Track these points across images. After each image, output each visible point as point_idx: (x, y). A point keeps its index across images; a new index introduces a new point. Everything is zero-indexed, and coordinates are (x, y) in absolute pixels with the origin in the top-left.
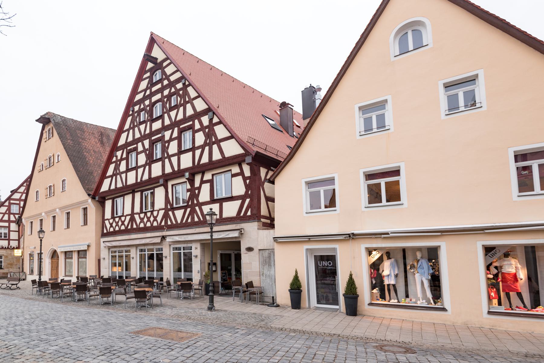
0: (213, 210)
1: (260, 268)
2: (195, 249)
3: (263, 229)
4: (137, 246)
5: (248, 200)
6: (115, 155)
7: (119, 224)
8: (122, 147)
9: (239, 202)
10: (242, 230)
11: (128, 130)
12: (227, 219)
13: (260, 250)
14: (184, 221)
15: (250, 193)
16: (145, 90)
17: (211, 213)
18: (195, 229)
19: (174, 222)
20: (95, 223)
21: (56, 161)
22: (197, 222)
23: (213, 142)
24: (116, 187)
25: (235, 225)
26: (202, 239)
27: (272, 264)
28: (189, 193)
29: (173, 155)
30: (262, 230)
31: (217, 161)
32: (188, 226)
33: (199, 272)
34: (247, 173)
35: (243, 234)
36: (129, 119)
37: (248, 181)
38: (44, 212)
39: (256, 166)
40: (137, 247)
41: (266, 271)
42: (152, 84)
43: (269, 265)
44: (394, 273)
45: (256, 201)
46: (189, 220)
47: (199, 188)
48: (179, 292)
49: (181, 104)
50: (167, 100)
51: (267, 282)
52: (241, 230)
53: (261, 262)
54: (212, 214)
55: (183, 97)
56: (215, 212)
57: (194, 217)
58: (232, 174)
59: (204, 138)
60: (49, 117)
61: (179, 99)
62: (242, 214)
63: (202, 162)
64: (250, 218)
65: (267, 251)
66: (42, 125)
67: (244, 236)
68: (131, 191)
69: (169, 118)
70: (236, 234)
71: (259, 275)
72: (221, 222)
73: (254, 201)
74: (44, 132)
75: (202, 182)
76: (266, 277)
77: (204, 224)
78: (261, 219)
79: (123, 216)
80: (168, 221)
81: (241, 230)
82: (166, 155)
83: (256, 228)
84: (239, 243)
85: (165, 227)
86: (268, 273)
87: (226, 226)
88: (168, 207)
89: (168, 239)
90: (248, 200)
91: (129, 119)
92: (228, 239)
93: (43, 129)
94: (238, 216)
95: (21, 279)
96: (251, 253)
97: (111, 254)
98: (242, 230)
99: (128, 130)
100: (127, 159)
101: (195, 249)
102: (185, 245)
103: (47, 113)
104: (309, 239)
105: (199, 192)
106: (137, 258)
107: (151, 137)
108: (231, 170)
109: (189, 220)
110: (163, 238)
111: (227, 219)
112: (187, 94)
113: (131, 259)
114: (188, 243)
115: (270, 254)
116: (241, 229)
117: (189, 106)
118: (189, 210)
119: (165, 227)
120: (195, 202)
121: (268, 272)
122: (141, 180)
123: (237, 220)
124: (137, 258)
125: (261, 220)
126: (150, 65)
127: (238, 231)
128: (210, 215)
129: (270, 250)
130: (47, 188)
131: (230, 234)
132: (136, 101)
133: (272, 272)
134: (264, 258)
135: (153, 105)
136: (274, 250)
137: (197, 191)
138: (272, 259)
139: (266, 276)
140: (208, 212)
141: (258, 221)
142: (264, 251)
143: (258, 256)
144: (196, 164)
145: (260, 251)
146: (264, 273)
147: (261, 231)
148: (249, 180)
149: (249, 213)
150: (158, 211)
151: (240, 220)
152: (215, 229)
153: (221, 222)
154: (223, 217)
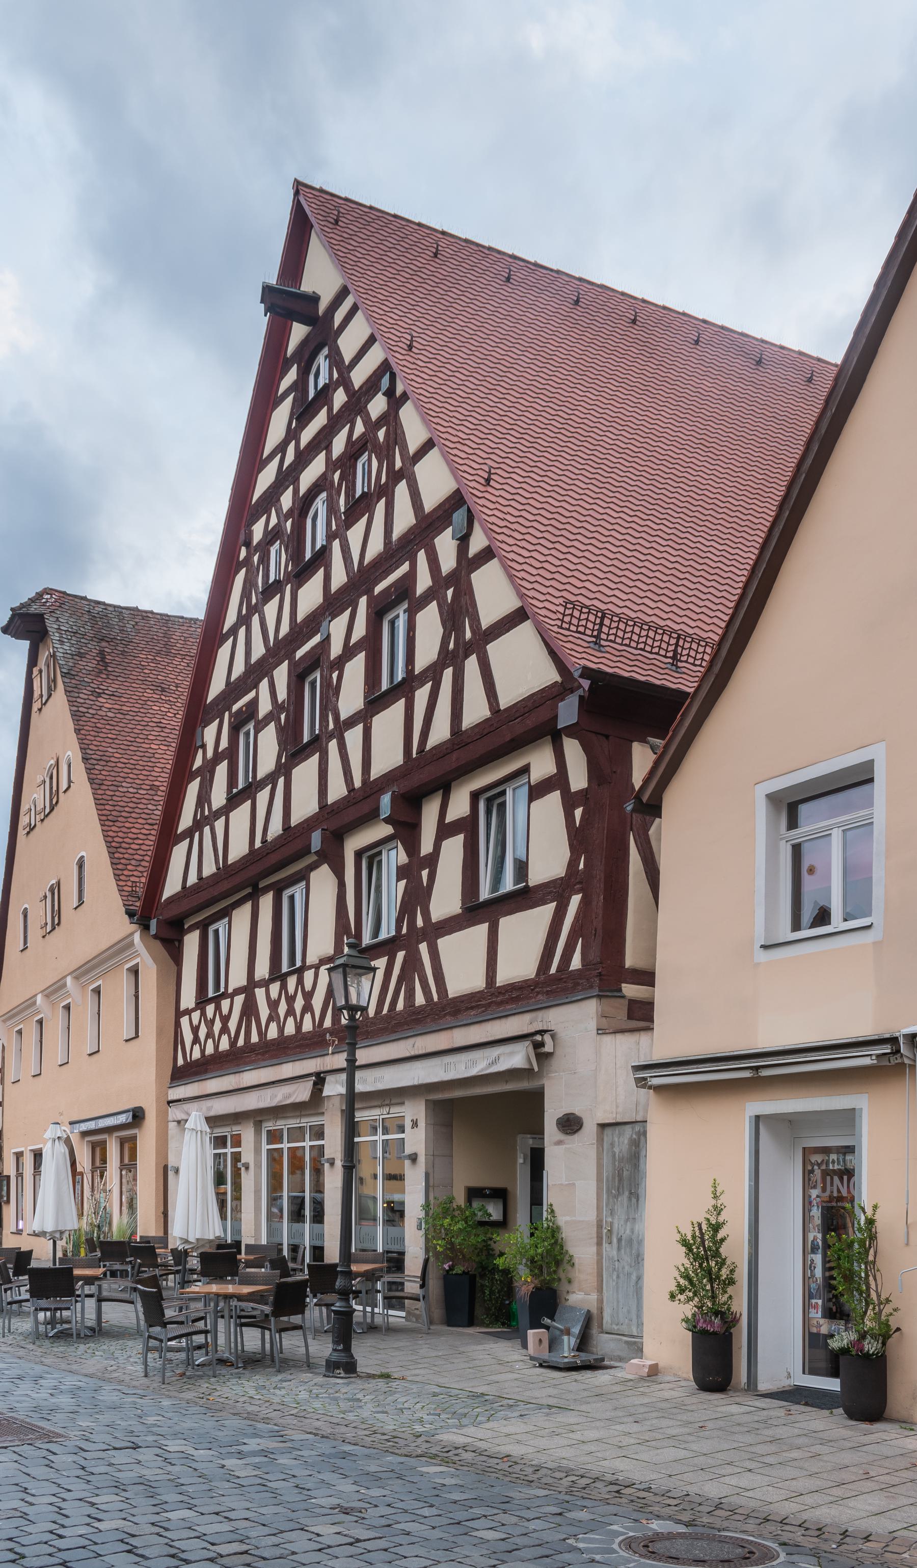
1: (599, 1209)
2: (413, 1128)
3: (614, 1033)
4: (257, 1116)
6: (199, 743)
7: (220, 1025)
8: (217, 705)
9: (547, 911)
10: (547, 1038)
11: (234, 631)
12: (507, 991)
13: (603, 1126)
14: (385, 1011)
15: (581, 866)
16: (281, 448)
20: (157, 1027)
21: (64, 785)
23: (466, 643)
24: (200, 878)
25: (527, 1017)
26: (239, 1110)
28: (403, 883)
30: (613, 1035)
31: (477, 730)
32: (418, 1021)
34: (578, 780)
35: (549, 1055)
36: (240, 579)
38: (42, 992)
39: (607, 737)
40: (258, 1125)
41: (618, 1223)
42: (302, 414)
43: (631, 1193)
44: (321, 1236)
45: (600, 904)
46: (400, 1006)
47: (432, 861)
48: (369, 1309)
49: (380, 486)
50: (341, 478)
51: (623, 1268)
52: (538, 1038)
53: (607, 1180)
55: (385, 453)
58: (533, 783)
59: (441, 630)
60: (42, 610)
61: (375, 464)
63: (432, 742)
65: (628, 1129)
66: (25, 644)
67: (555, 1063)
69: (344, 557)
71: (595, 1240)
72: (489, 1005)
73: (594, 903)
74: (35, 671)
76: (619, 1249)
77: (440, 1018)
78: (623, 985)
79: (224, 995)
81: (538, 1038)
83: (592, 1025)
84: (536, 1099)
85: (328, 1037)
86: (628, 1232)
87: (503, 1021)
91: (240, 579)
93: (33, 661)
95: (180, 1256)
97: (265, 1147)
98: (547, 1038)
99: (234, 631)
100: (231, 754)
102: (293, 1123)
103: (39, 595)
104: (757, 1068)
106: (258, 1165)
107: (295, 651)
108: (526, 770)
109: (400, 1006)
111: (507, 991)
112: (399, 441)
113: (327, 1165)
114: (303, 1113)
116: (541, 1032)
119: (328, 1037)
122: (264, 841)
123: (538, 993)
124: (258, 1165)
125: (620, 990)
126: (298, 332)
127: (527, 1043)
130: (45, 897)
131: (502, 1059)
132: (357, 439)
135: (304, 505)
136: (645, 1127)
139: (620, 1240)
141: (599, 997)
142: (618, 1129)
143: (592, 1153)
145: (608, 1131)
146: (616, 1226)
147: (608, 1039)
149: (576, 962)
151: (548, 993)
152: (363, 1056)
153: (489, 1005)
154: (450, 996)
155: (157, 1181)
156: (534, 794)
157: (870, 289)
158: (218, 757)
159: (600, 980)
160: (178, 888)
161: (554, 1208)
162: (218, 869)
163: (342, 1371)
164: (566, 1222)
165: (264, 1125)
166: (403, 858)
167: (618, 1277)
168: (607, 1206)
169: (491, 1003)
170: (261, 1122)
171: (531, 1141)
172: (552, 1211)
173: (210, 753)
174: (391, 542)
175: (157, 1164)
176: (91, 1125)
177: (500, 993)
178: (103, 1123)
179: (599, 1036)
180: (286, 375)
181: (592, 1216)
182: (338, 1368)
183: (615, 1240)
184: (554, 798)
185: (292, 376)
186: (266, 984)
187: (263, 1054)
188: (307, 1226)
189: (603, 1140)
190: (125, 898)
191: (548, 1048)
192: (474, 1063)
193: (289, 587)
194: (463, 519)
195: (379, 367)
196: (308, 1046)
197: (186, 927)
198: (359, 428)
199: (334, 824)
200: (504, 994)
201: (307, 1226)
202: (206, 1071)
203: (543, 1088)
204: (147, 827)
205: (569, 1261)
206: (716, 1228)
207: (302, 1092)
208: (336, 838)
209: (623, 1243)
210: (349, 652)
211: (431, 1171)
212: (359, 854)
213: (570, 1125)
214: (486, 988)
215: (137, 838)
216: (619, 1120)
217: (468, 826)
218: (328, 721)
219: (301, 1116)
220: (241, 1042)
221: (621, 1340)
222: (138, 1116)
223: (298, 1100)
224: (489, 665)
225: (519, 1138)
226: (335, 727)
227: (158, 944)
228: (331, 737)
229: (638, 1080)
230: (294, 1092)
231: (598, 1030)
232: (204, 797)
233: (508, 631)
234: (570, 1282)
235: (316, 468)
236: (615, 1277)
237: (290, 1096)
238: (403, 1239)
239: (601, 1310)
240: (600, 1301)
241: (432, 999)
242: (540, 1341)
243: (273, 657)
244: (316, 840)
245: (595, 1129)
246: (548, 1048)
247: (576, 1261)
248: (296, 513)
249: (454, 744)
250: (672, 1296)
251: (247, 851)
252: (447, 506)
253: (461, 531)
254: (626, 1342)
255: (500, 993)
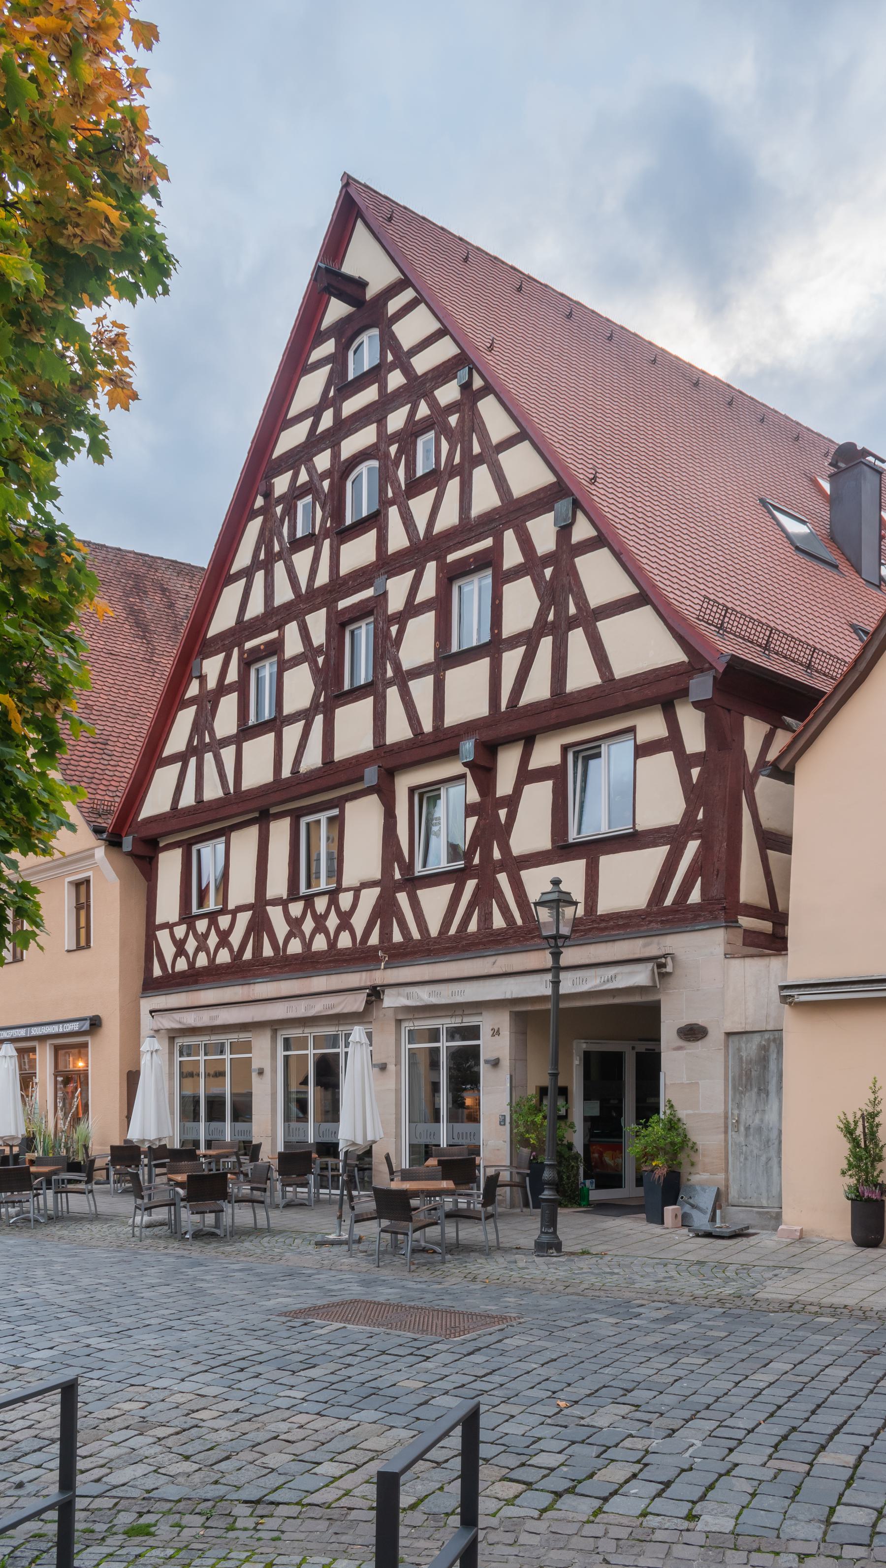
0: (563, 887)
1: (726, 1102)
2: (493, 1035)
3: (744, 957)
4: (275, 1026)
5: (693, 846)
6: (195, 673)
11: (248, 573)
13: (728, 1034)
14: (453, 930)
15: (700, 816)
16: (316, 412)
17: (554, 896)
18: (492, 959)
19: (416, 935)
22: (500, 931)
24: (199, 800)
25: (640, 942)
27: (772, 1087)
28: (472, 821)
29: (418, 672)
30: (742, 960)
33: (502, 1122)
35: (668, 974)
36: (254, 527)
37: (695, 772)
39: (729, 710)
40: (275, 1032)
43: (760, 1090)
45: (723, 849)
46: (473, 927)
47: (512, 802)
50: (399, 452)
51: (752, 1151)
52: (663, 960)
54: (557, 902)
56: (569, 894)
57: (491, 913)
62: (669, 901)
64: (700, 916)
65: (756, 1039)
67: (672, 981)
68: (257, 815)
69: (404, 524)
70: (640, 976)
71: (723, 1129)
72: (590, 930)
73: (716, 849)
75: (525, 776)
76: (747, 1136)
77: (527, 940)
78: (739, 917)
79: (223, 911)
80: (392, 931)
81: (663, 960)
82: (390, 673)
83: (720, 950)
86: (757, 1121)
88: (393, 876)
89: (391, 1000)
90: (693, 846)
91: (254, 527)
92: (614, 997)
94: (655, 909)
96: (697, 1048)
99: (248, 573)
101: (493, 1035)
105: (512, 817)
109: (473, 927)
110: (375, 994)
111: (612, 919)
112: (476, 426)
114: (457, 1013)
115: (765, 1049)
116: (665, 956)
117: (481, 475)
118: (471, 885)
120: (497, 854)
121: (758, 1116)
122: (295, 771)
123: (651, 922)
125: (737, 922)
127: (650, 965)
128: (552, 904)
129: (767, 1036)
131: (619, 977)
133: (771, 1117)
134: (744, 1065)
137: (503, 813)
138: (773, 1066)
139: (747, 1128)
140: (543, 894)
141: (726, 927)
142: (744, 1037)
144: (504, 706)
145: (731, 1039)
146: (743, 1117)
148: (698, 769)
149: (695, 897)
150: (357, 891)
151: (662, 922)
153: (590, 930)
155: (121, 1087)
156: (640, 752)
157: (334, 205)
158: (222, 689)
159: (726, 913)
160: (166, 808)
161: (673, 1103)
162: (227, 793)
163: (554, 1251)
164: (687, 1115)
165: (279, 1033)
166: (474, 796)
167: (746, 1159)
168: (733, 1100)
169: (593, 928)
170: (276, 1030)
171: (584, 1046)
172: (672, 1107)
173: (212, 684)
174: (469, 517)
175: (121, 1070)
176: (22, 1033)
177: (603, 920)
178: (36, 1031)
179: (726, 960)
180: (319, 346)
181: (720, 1109)
182: (551, 1248)
183: (742, 1129)
184: (667, 758)
185: (328, 347)
186: (284, 903)
187: (281, 967)
188: (202, 1124)
189: (728, 1046)
190: (86, 814)
191: (669, 969)
192: (584, 981)
193: (327, 542)
194: (567, 510)
195: (449, 360)
196: (345, 961)
197: (161, 845)
198: (423, 410)
199: (390, 763)
200: (607, 921)
201: (202, 1124)
202: (196, 982)
203: (659, 1002)
204: (90, 745)
205: (692, 1148)
206: (873, 1115)
207: (356, 1003)
208: (389, 775)
209: (751, 1130)
210: (412, 609)
211: (513, 1074)
212: (412, 791)
213: (695, 1034)
214: (585, 915)
215: (84, 756)
216: (748, 1029)
217: (556, 774)
218: (386, 669)
219: (339, 1025)
220: (248, 955)
221: (751, 1211)
222: (95, 1023)
223: (346, 1011)
224: (600, 639)
225: (575, 1043)
226: (395, 675)
227: (130, 862)
228: (390, 683)
229: (784, 999)
230: (339, 1004)
231: (725, 954)
232: (204, 723)
233: (623, 612)
234: (693, 1164)
235: (366, 437)
236: (742, 1159)
237: (333, 1007)
238: (250, 1132)
239: (727, 1187)
240: (727, 1179)
241: (515, 923)
242: (676, 1216)
243: (76, 568)
244: (371, 775)
245: (723, 1036)
246: (669, 969)
247: (700, 1148)
248: (336, 476)
249: (555, 703)
250: (843, 1173)
251: (271, 779)
252: (542, 495)
253: (565, 520)
254: (758, 1212)
255: (603, 920)
